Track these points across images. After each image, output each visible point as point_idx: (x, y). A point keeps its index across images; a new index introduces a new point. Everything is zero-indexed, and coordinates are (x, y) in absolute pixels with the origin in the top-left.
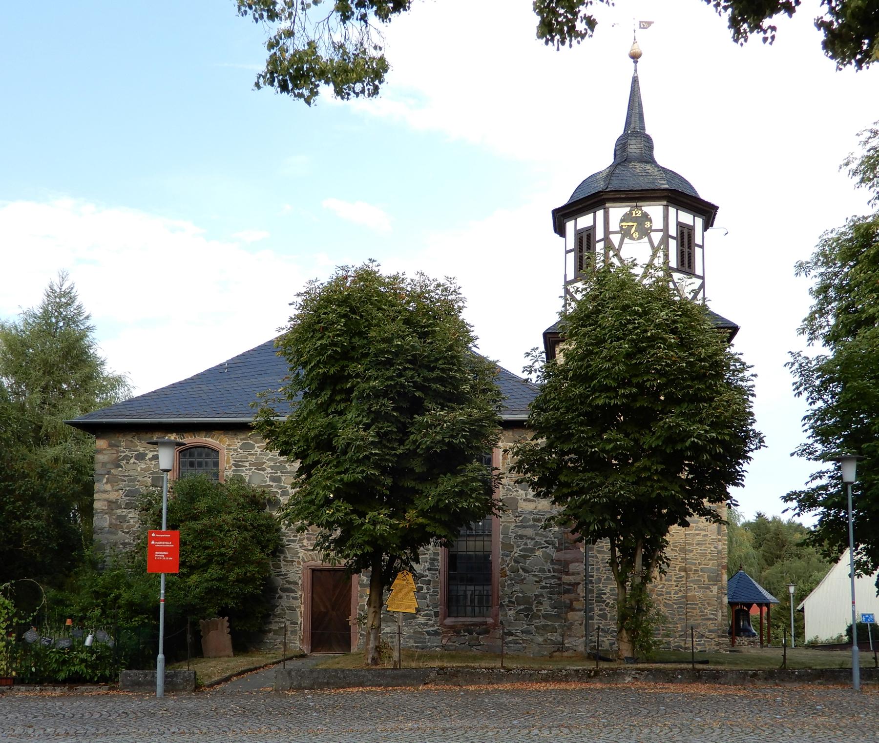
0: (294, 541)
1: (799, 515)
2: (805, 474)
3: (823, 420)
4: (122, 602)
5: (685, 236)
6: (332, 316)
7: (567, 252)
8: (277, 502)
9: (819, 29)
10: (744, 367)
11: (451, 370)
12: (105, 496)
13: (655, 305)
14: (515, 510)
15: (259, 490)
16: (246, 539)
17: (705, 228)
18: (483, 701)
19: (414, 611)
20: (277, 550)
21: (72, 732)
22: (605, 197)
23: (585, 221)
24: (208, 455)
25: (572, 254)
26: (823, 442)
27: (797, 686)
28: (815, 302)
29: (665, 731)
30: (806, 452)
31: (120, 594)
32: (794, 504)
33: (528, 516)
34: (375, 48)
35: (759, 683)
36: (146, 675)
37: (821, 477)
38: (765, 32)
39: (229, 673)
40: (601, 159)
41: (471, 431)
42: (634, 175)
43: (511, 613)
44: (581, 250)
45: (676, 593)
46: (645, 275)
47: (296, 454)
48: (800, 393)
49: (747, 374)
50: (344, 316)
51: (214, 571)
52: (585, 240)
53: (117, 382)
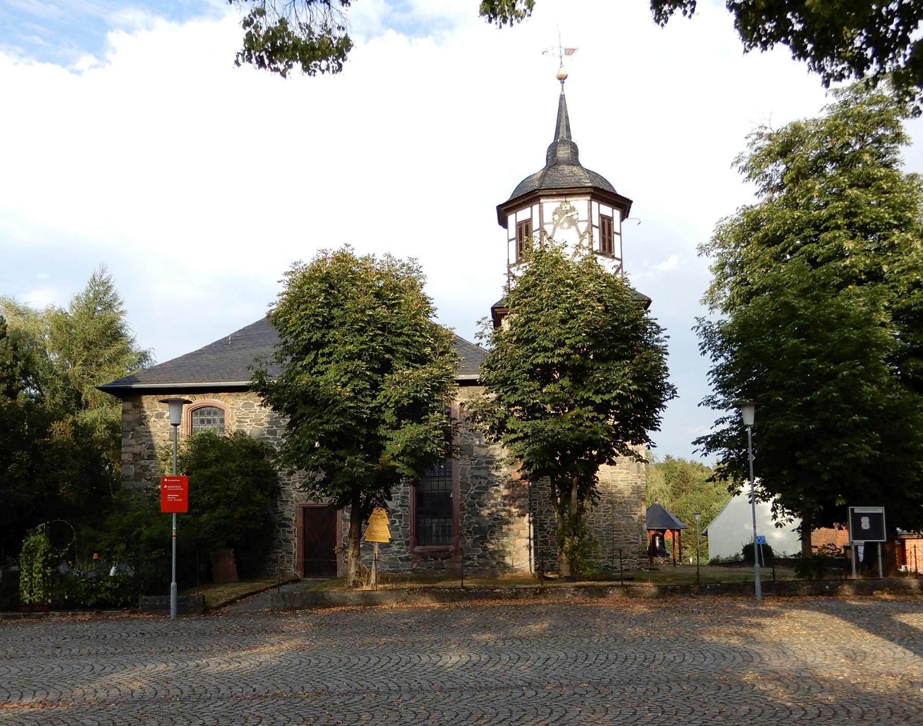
0: (288, 484)
1: (706, 454)
2: (710, 421)
3: (724, 374)
4: (143, 538)
5: (606, 225)
6: (314, 291)
7: (510, 240)
8: (274, 451)
9: (731, 11)
10: (659, 330)
11: (414, 335)
12: (130, 449)
13: (585, 278)
14: (471, 455)
15: (258, 442)
16: (247, 483)
17: (622, 219)
18: (446, 617)
19: (388, 541)
20: (274, 491)
21: (93, 652)
22: (540, 193)
23: (523, 214)
24: (215, 413)
25: (514, 242)
26: (723, 393)
27: (708, 599)
28: (714, 277)
29: (602, 641)
30: (710, 402)
31: (142, 532)
32: (703, 445)
33: (482, 460)
34: (339, 28)
35: (677, 596)
36: (161, 600)
37: (723, 422)
38: (685, 6)
39: (233, 596)
40: (536, 164)
41: (433, 387)
42: (563, 176)
43: (470, 541)
44: (521, 238)
45: (604, 522)
46: (575, 254)
47: (286, 409)
48: (704, 352)
49: (661, 336)
50: (324, 291)
51: (222, 510)
52: (524, 229)
53: (144, 356)
